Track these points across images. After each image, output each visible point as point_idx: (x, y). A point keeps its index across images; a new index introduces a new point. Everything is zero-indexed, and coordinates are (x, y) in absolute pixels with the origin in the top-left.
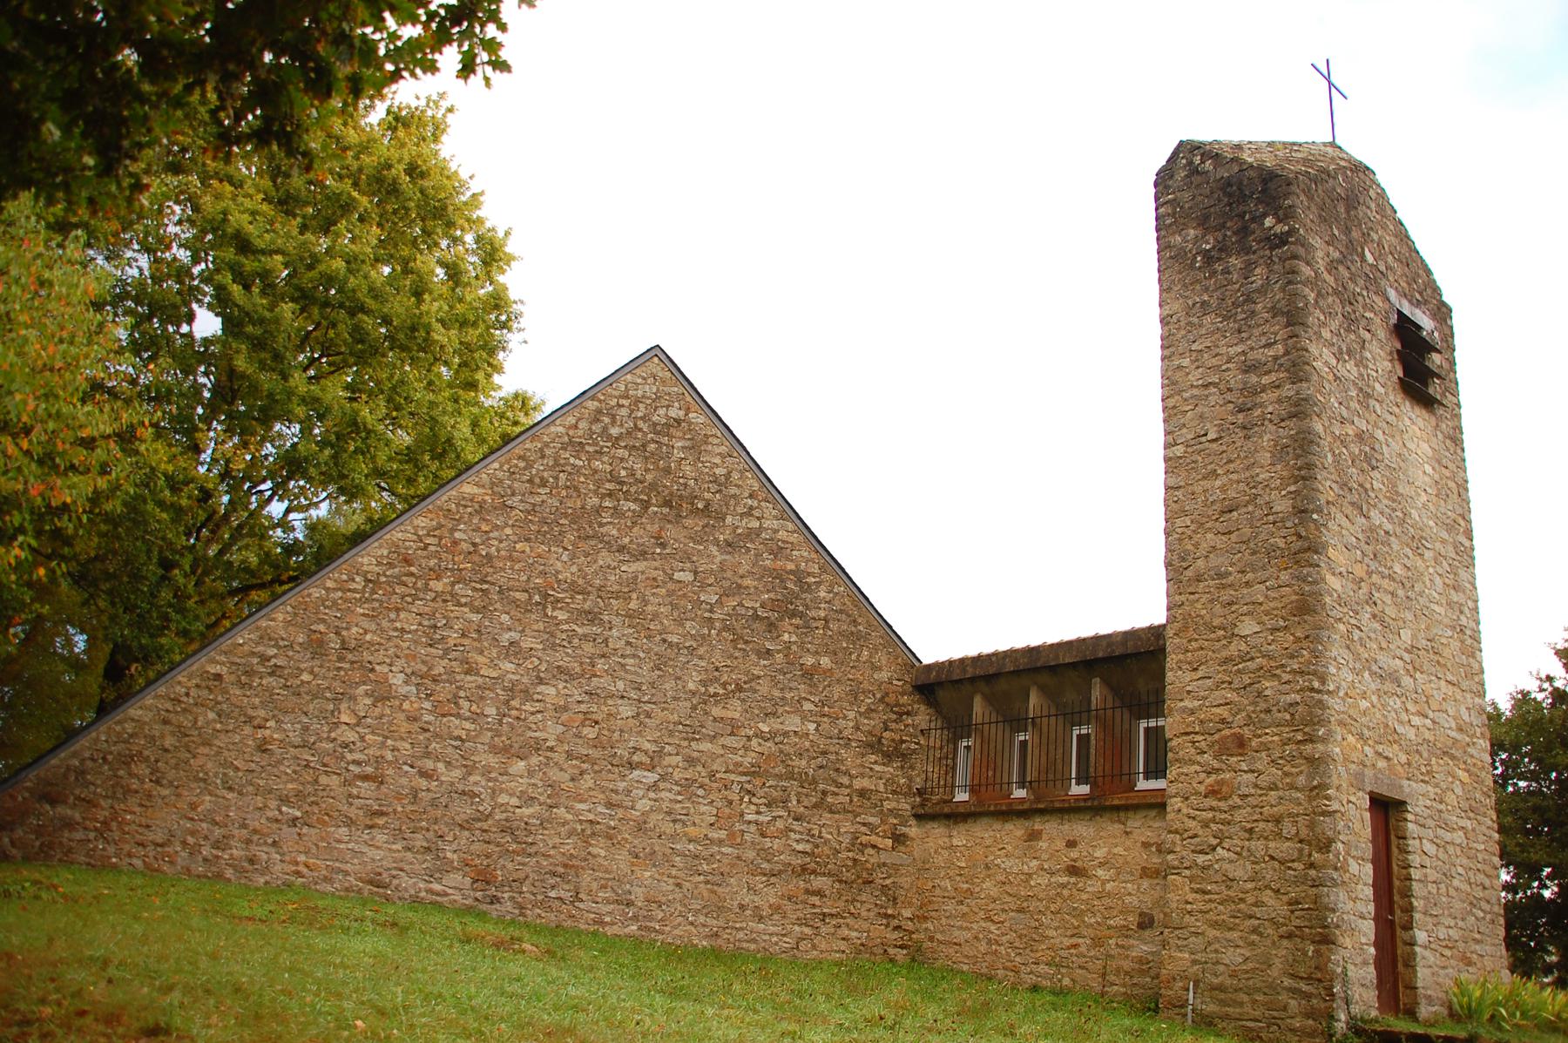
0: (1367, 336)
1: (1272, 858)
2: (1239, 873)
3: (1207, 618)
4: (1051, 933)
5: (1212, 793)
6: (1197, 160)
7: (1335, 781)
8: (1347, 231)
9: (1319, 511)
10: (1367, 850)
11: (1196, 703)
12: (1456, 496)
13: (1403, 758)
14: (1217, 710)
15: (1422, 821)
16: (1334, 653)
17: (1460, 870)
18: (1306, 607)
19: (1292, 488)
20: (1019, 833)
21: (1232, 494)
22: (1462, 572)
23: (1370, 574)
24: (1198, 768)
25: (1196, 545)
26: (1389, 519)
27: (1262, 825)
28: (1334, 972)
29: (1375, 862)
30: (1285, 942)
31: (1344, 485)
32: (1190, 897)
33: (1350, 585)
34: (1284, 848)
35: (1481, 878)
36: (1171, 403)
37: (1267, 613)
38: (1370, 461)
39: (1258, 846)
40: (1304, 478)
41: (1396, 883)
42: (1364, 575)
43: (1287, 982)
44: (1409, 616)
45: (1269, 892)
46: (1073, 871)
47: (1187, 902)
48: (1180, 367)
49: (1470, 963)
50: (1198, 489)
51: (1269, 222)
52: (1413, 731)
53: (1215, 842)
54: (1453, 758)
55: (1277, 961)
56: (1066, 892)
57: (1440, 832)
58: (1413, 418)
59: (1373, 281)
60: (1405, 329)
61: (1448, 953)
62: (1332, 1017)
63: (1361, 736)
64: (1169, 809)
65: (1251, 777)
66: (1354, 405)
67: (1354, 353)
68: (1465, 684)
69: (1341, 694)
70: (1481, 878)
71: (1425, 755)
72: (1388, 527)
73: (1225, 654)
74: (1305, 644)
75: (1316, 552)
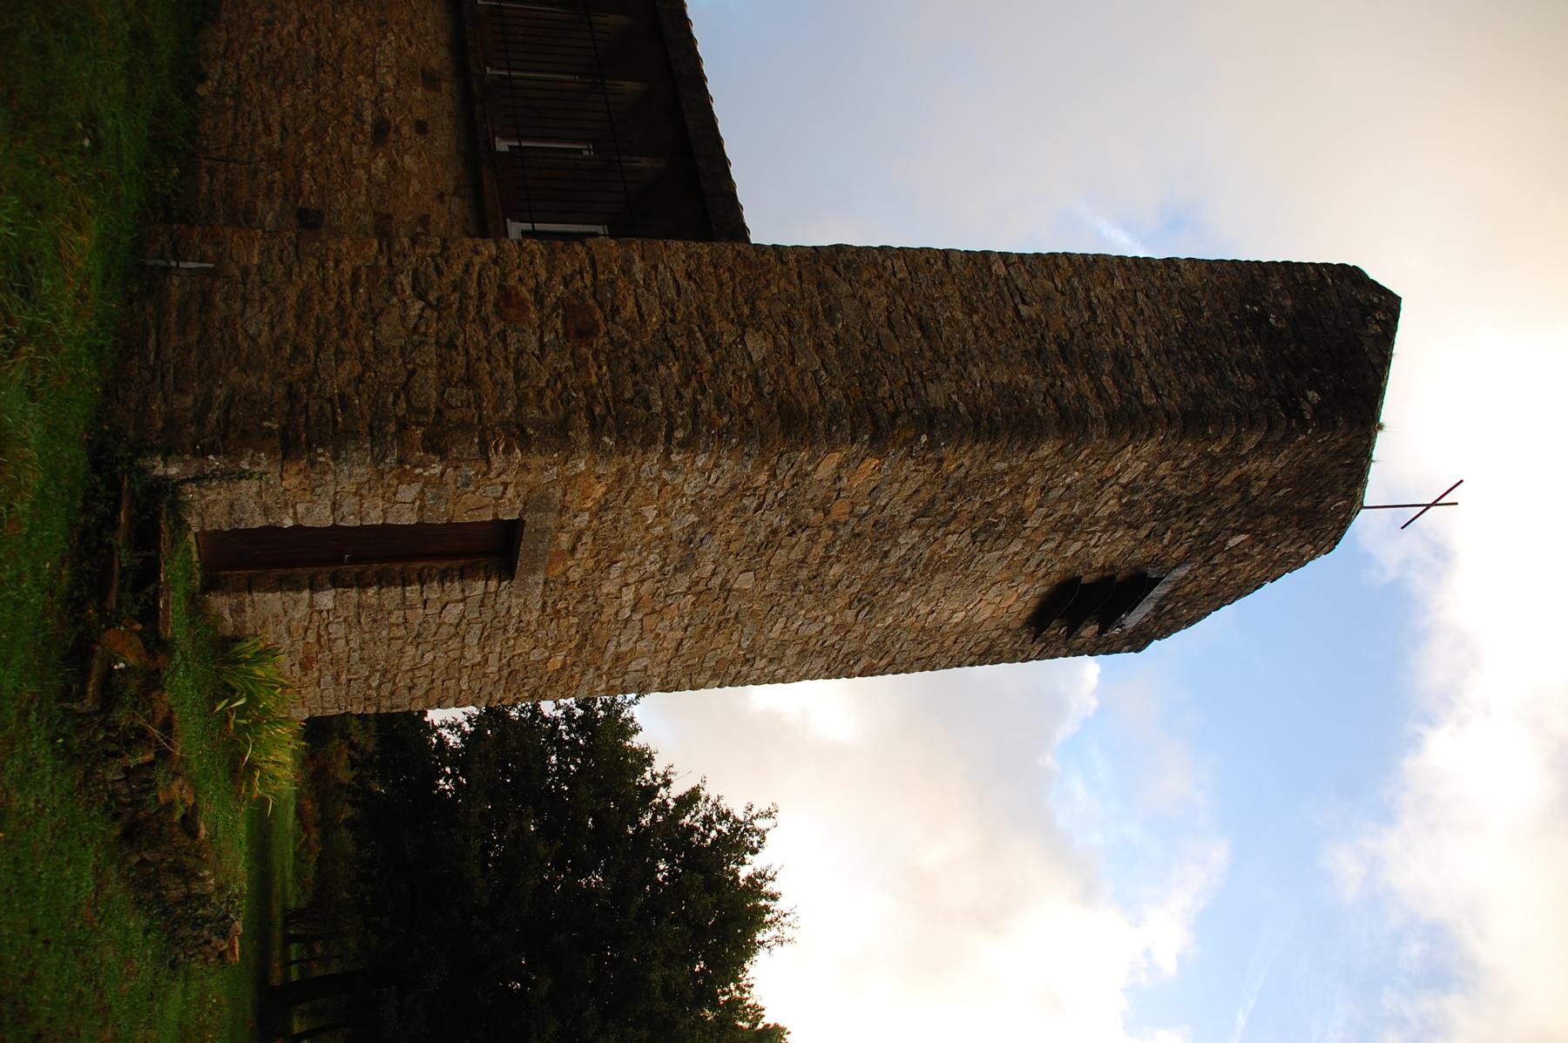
0: (1143, 533)
1: (412, 373)
2: (385, 330)
3: (765, 293)
4: (287, 101)
5: (507, 297)
6: (1380, 316)
7: (536, 461)
8: (1276, 510)
9: (932, 445)
10: (439, 515)
11: (640, 277)
12: (918, 654)
13: (575, 575)
14: (631, 303)
15: (489, 602)
16: (727, 464)
17: (429, 656)
18: (789, 423)
19: (962, 408)
20: (434, 63)
21: (946, 332)
22: (822, 661)
23: (834, 526)
24: (543, 277)
25: (869, 284)
26: (904, 559)
27: (461, 360)
28: (241, 456)
29: (420, 530)
30: (281, 391)
31: (960, 486)
32: (346, 267)
33: (821, 493)
34: (428, 387)
35: (423, 684)
36: (1064, 263)
37: (780, 371)
38: (986, 533)
39: (430, 354)
40: (977, 424)
41: (398, 567)
42: (833, 517)
43: (220, 393)
44: (771, 586)
45: (359, 369)
46: (381, 131)
47: (337, 262)
48: (1111, 276)
49: (306, 666)
50: (949, 289)
51: (1313, 395)
52: (613, 589)
53: (432, 297)
54: (580, 647)
55: (253, 380)
56: (349, 119)
57: (477, 629)
58: (1013, 599)
59: (1206, 546)
60: (1134, 585)
61: (312, 638)
62: (168, 453)
63: (603, 507)
64: (479, 241)
65: (533, 345)
66: (1062, 509)
67: (1125, 519)
68: (677, 665)
69: (665, 475)
70: (423, 684)
71: (581, 608)
72: (893, 559)
73: (715, 314)
74: (738, 420)
75: (873, 439)
